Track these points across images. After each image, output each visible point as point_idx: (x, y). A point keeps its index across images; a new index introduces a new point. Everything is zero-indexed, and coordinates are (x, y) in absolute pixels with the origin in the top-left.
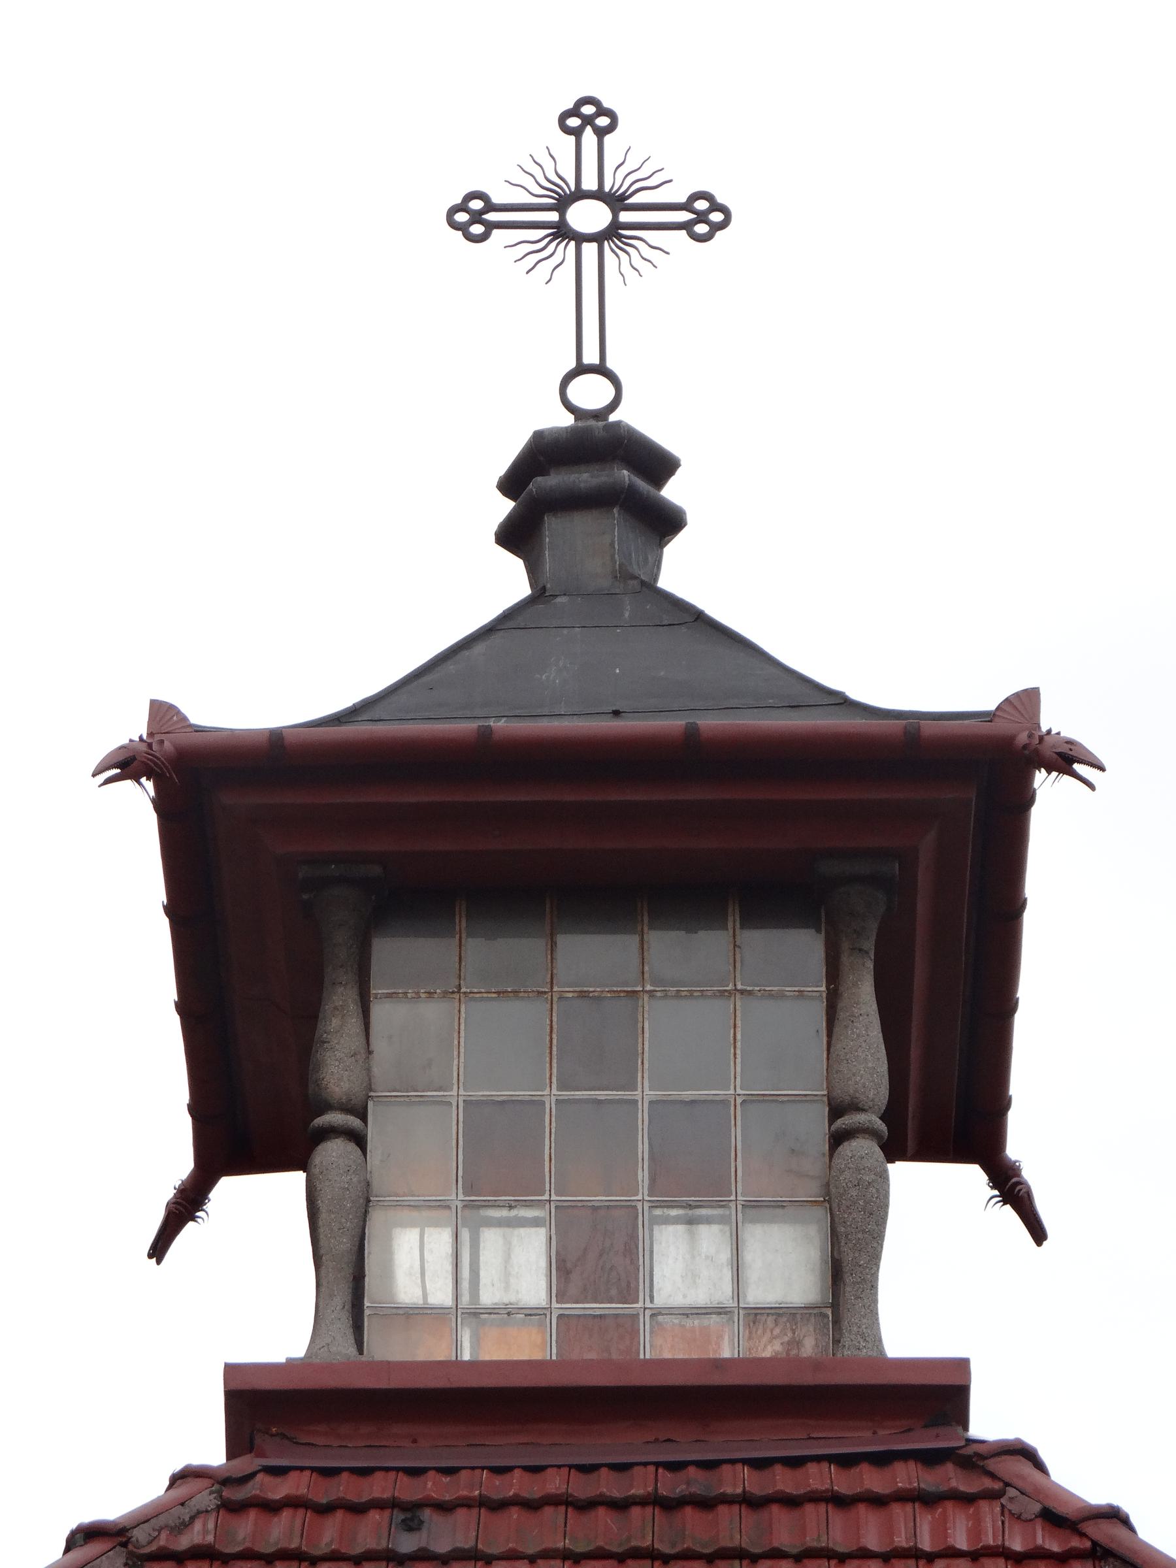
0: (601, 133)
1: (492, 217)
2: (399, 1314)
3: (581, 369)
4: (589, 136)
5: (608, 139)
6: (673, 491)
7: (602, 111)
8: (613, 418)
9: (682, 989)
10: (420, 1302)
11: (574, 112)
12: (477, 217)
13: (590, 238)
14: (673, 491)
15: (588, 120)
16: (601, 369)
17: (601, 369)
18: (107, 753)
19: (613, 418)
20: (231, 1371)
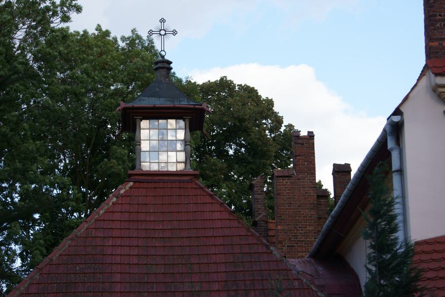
1: (153, 33)
16: (164, 51)
17: (164, 51)
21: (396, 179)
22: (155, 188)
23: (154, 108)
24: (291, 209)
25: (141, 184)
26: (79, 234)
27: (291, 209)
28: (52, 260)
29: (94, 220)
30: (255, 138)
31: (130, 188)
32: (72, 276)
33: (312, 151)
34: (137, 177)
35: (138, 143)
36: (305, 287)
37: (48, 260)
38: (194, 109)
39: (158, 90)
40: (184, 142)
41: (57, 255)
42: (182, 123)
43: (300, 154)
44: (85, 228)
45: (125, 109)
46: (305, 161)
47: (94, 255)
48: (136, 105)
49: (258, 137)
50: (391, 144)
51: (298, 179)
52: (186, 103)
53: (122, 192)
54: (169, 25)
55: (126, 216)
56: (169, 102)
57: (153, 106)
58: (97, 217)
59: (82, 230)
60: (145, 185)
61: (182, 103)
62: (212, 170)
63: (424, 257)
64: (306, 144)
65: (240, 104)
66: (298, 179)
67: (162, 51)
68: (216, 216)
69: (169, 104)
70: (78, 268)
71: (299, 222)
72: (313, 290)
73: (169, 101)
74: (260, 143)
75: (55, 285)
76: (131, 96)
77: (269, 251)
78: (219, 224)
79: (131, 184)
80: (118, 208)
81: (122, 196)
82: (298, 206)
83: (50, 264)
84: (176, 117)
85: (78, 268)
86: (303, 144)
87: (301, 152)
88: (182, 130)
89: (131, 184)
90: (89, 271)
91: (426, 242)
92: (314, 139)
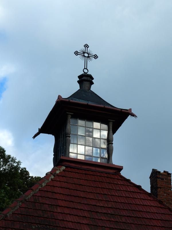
0: (87, 48)
1: (78, 53)
2: (83, 224)
3: (85, 68)
4: (86, 48)
5: (88, 48)
6: (93, 81)
7: (88, 46)
8: (87, 73)
9: (111, 120)
10: (91, 160)
11: (85, 45)
12: (77, 53)
13: (86, 53)
14: (93, 81)
15: (86, 46)
16: (87, 69)
17: (87, 69)
18: (50, 111)
19: (87, 73)
20: (153, 169)
26: (27, 198)
28: (6, 216)
29: (38, 190)
31: (64, 170)
33: (169, 186)
34: (68, 164)
35: (69, 135)
37: (3, 215)
40: (106, 141)
42: (105, 126)
43: (161, 186)
44: (32, 195)
46: (165, 193)
47: (46, 218)
54: (92, 50)
58: (40, 187)
59: (29, 196)
64: (165, 179)
67: (85, 68)
79: (64, 168)
81: (58, 175)
83: (4, 220)
84: (102, 121)
86: (162, 179)
87: (162, 185)
88: (106, 131)
89: (64, 168)
92: (171, 176)
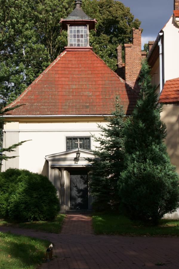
21: (161, 56)
22: (75, 54)
23: (75, 21)
24: (131, 60)
25: (70, 52)
27: (131, 60)
30: (122, 26)
31: (66, 54)
32: (43, 89)
36: (133, 94)
38: (91, 21)
39: (76, 13)
41: (38, 81)
45: (63, 21)
48: (67, 20)
49: (123, 25)
50: (160, 44)
51: (134, 48)
52: (87, 19)
53: (62, 55)
55: (64, 65)
56: (81, 18)
57: (74, 20)
58: (52, 65)
60: (71, 53)
61: (86, 19)
62: (104, 40)
63: (168, 86)
65: (115, 10)
66: (134, 48)
68: (99, 65)
69: (82, 20)
70: (45, 86)
71: (134, 66)
72: (135, 95)
73: (81, 18)
74: (124, 27)
75: (37, 92)
76: (9, 207)
77: (119, 80)
78: (100, 69)
80: (61, 62)
82: (134, 59)
85: (45, 86)
89: (66, 52)
90: (49, 87)
91: (170, 81)
